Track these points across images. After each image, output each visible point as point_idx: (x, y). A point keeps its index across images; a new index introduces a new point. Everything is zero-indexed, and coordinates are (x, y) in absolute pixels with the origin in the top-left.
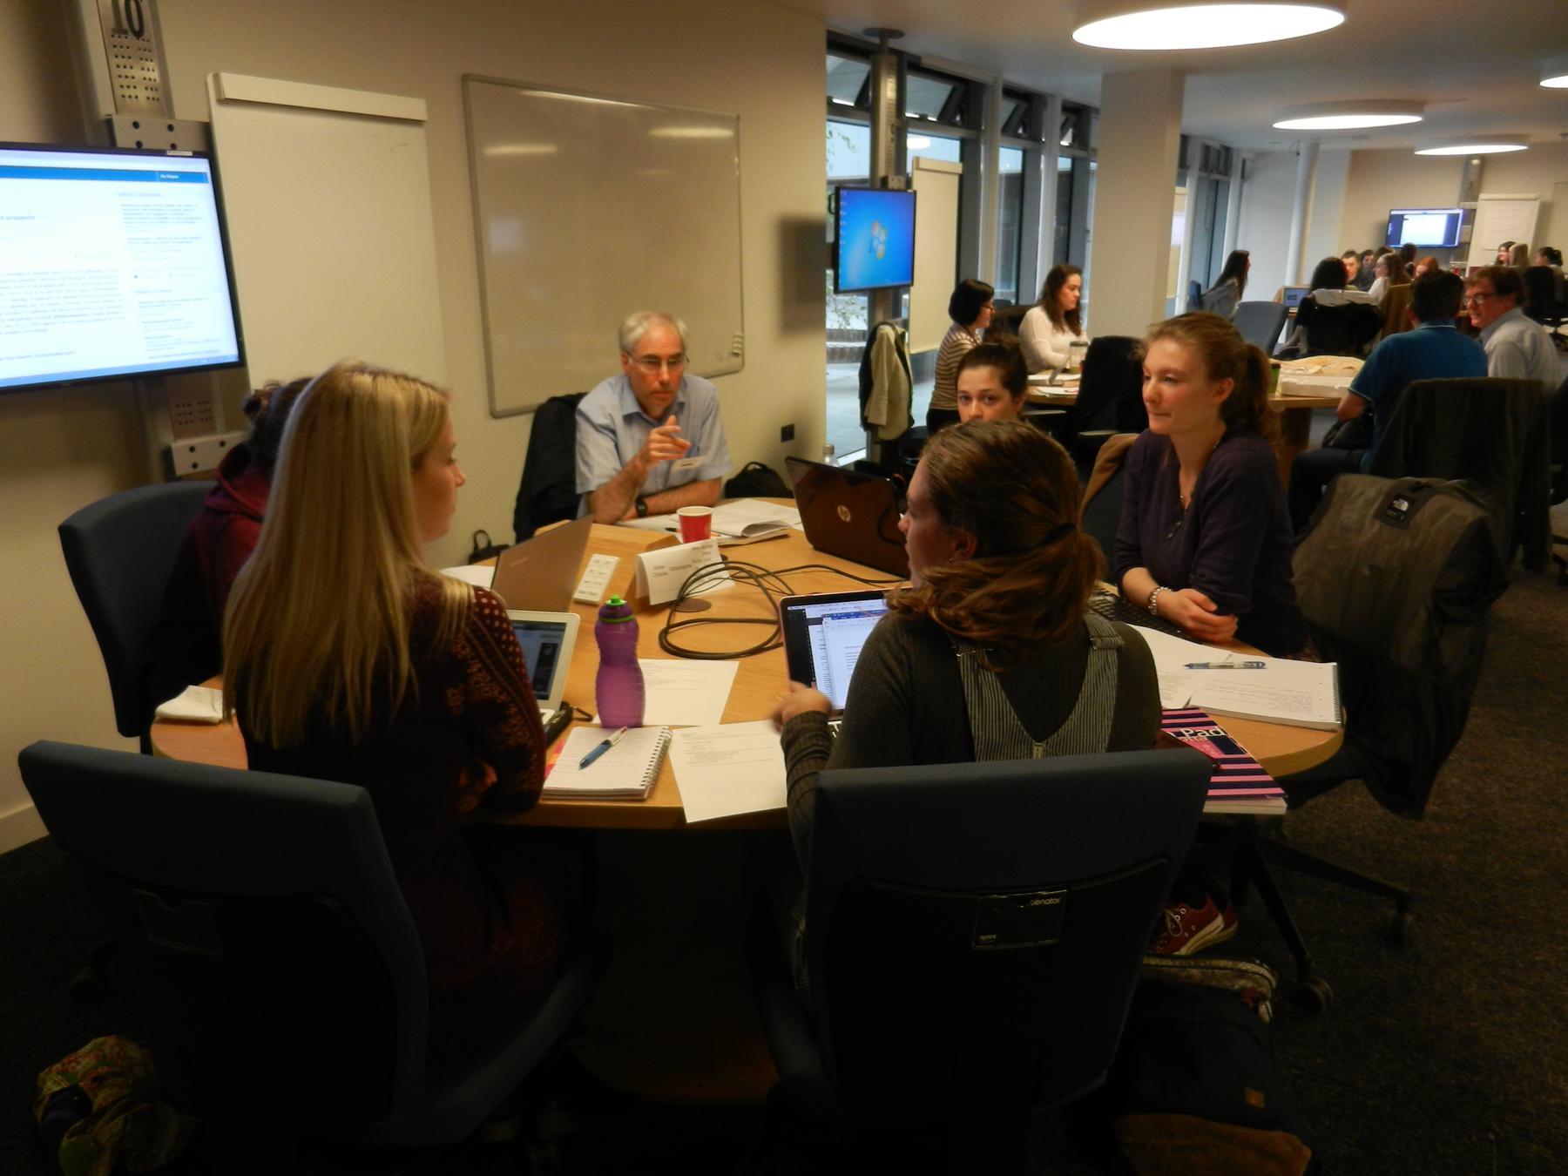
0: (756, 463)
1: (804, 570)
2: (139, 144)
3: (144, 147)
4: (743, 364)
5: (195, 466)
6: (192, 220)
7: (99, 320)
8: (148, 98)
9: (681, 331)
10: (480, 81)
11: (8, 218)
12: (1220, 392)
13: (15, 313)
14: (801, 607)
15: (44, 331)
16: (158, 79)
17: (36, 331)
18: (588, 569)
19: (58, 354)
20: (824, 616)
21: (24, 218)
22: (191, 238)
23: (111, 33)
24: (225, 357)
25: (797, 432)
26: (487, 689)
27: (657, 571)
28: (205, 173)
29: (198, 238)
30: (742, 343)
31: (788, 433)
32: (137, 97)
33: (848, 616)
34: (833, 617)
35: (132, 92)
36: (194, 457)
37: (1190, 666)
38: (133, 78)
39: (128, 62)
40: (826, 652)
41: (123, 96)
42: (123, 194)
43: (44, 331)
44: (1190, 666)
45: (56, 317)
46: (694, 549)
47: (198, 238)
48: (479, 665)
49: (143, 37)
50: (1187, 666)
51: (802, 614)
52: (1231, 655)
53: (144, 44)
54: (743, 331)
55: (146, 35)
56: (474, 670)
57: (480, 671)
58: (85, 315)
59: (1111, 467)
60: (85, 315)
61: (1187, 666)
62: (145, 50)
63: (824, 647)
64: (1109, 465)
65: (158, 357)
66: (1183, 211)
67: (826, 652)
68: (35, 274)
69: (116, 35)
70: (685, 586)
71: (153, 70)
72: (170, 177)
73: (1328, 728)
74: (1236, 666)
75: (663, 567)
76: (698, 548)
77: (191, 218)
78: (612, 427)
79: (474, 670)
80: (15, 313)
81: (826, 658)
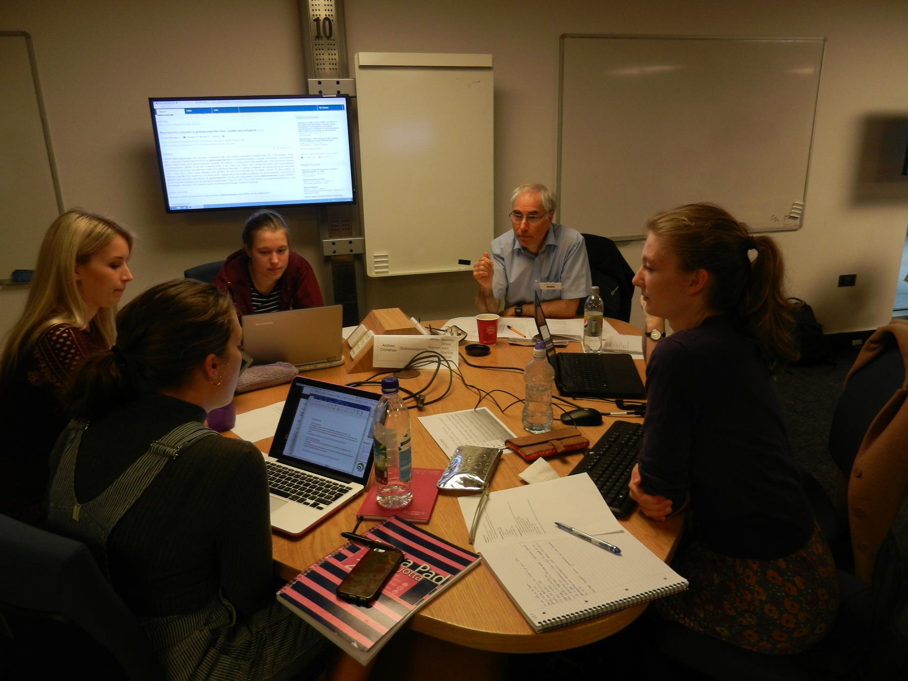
0: (797, 299)
1: (511, 370)
2: (339, 92)
3: (341, 93)
4: (801, 225)
5: (351, 251)
6: (334, 129)
7: (283, 178)
8: (330, 69)
9: (543, 194)
10: (572, 37)
11: (245, 131)
12: (695, 282)
13: (244, 174)
14: (302, 385)
15: (257, 182)
16: (337, 59)
17: (242, 183)
18: (623, 349)
19: (262, 193)
20: (311, 395)
21: (251, 130)
22: (333, 138)
23: (315, 38)
24: (346, 199)
25: (857, 280)
26: (49, 378)
27: (384, 348)
28: (344, 105)
29: (337, 138)
30: (803, 210)
31: (847, 281)
32: (324, 69)
33: (323, 398)
34: (317, 397)
35: (322, 67)
36: (351, 246)
37: (559, 526)
38: (323, 59)
39: (321, 52)
40: (302, 418)
41: (318, 69)
42: (300, 118)
43: (257, 182)
44: (559, 526)
45: (262, 176)
46: (432, 339)
47: (337, 138)
48: (45, 364)
49: (331, 38)
50: (556, 523)
51: (301, 389)
52: (622, 532)
53: (332, 42)
54: (804, 200)
55: (333, 37)
56: (42, 366)
57: (45, 367)
58: (276, 175)
59: (874, 349)
60: (276, 175)
61: (556, 523)
62: (331, 45)
63: (302, 414)
64: (873, 345)
65: (310, 197)
66: (344, 109)
67: (302, 418)
68: (254, 156)
69: (317, 40)
70: (413, 361)
71: (335, 55)
72: (323, 108)
73: (532, 626)
74: (592, 541)
75: (394, 346)
76: (438, 340)
77: (333, 128)
78: (502, 256)
79: (42, 366)
80: (244, 174)
81: (300, 422)
